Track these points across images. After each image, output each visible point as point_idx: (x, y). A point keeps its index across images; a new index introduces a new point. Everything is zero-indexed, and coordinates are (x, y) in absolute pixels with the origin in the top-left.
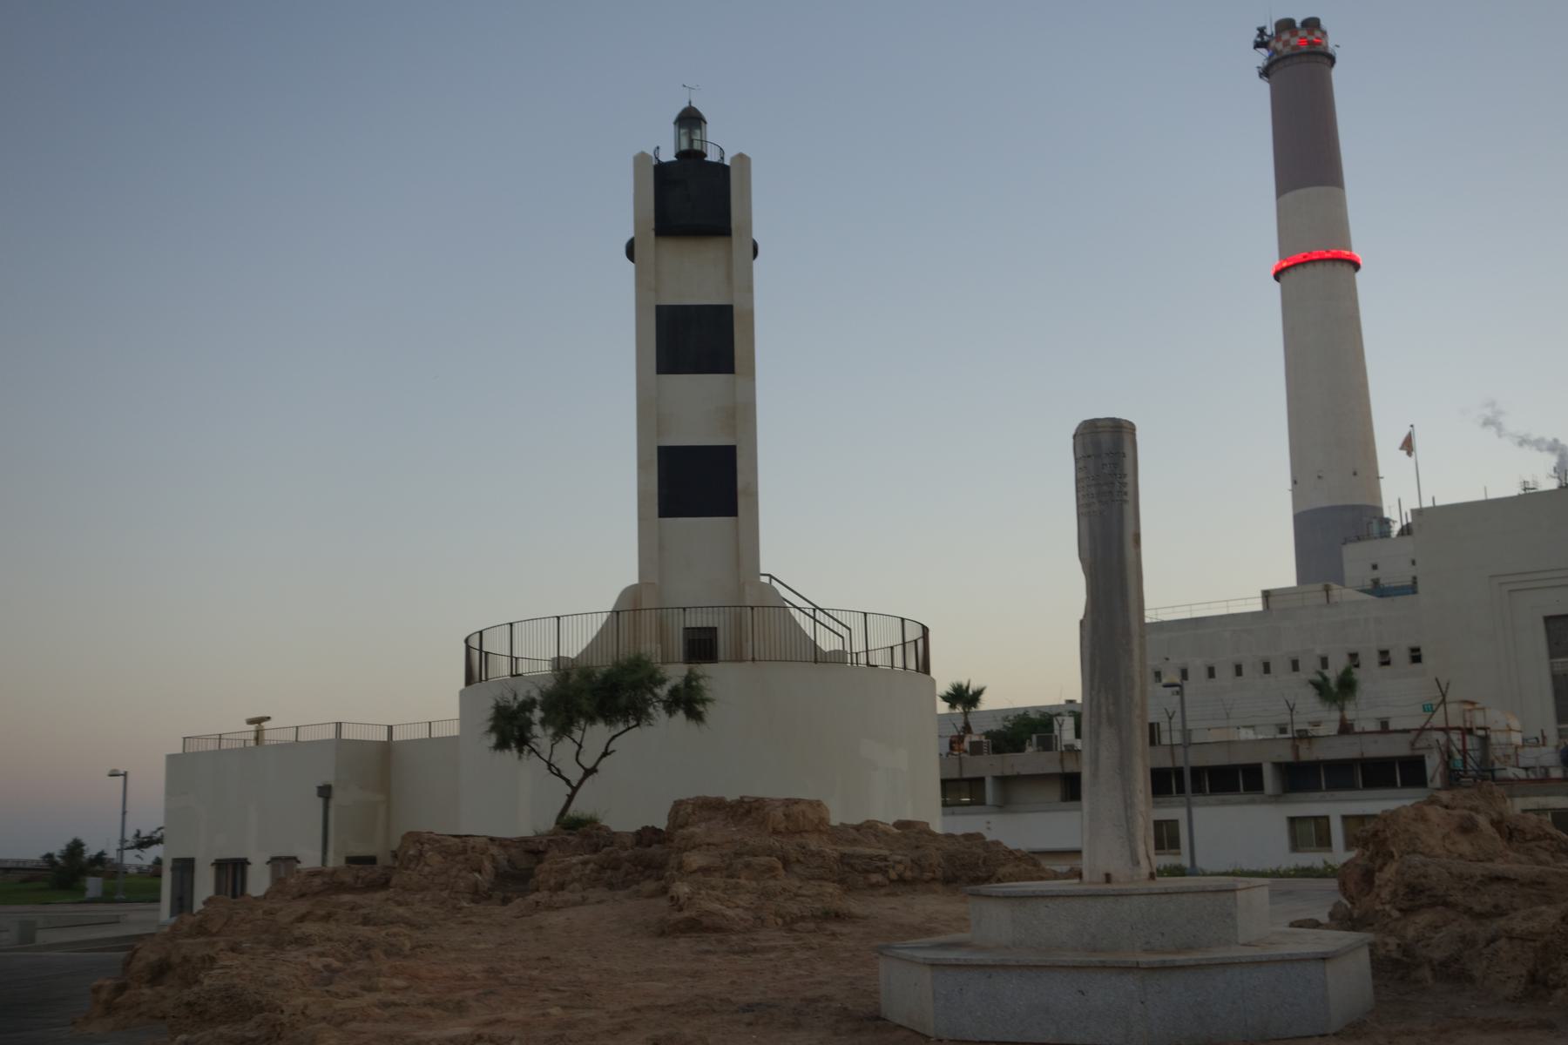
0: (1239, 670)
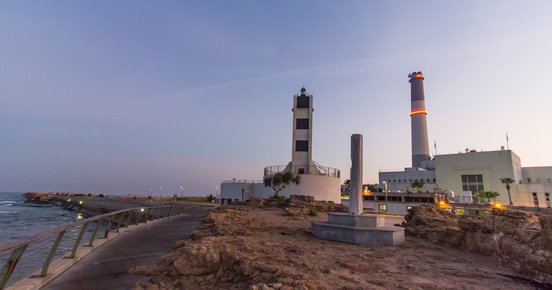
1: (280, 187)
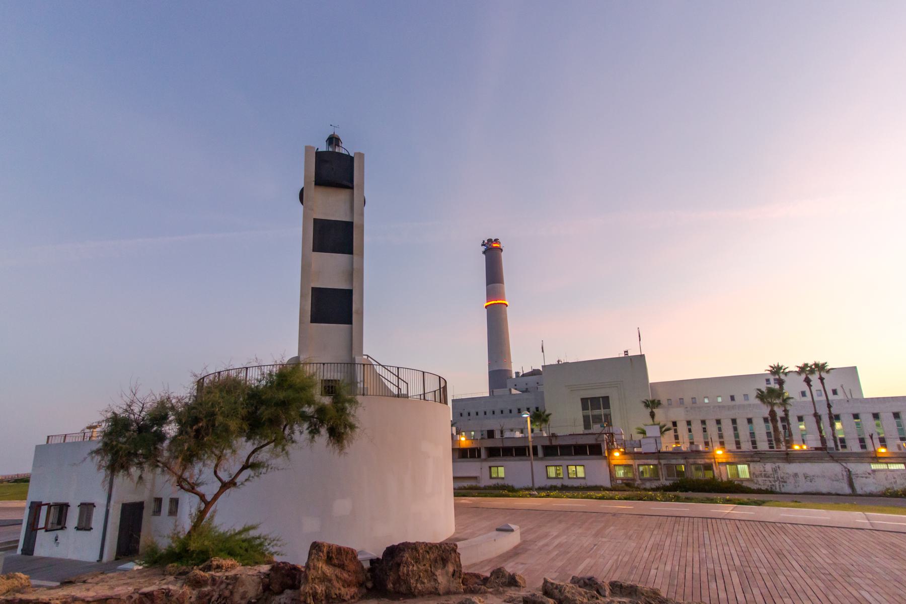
0: (485, 413)
1: (231, 465)
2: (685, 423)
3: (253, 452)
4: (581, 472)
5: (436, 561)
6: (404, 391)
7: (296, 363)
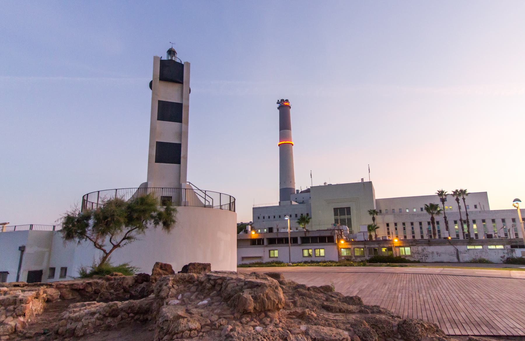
1: (118, 238)
2: (394, 224)
3: (128, 232)
4: (322, 252)
5: (201, 269)
6: (211, 204)
7: (144, 187)
